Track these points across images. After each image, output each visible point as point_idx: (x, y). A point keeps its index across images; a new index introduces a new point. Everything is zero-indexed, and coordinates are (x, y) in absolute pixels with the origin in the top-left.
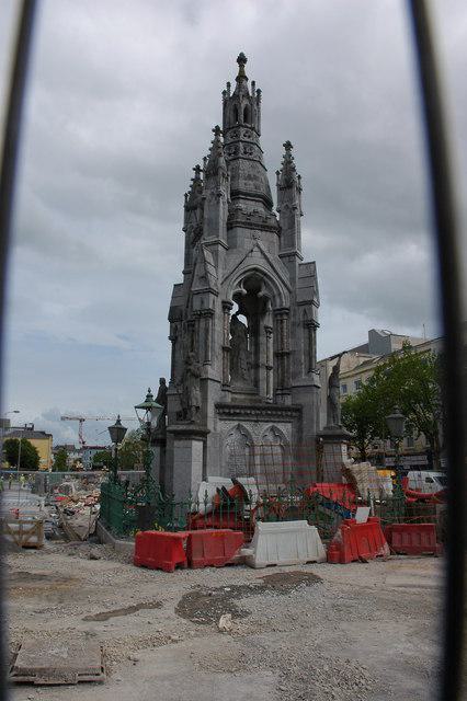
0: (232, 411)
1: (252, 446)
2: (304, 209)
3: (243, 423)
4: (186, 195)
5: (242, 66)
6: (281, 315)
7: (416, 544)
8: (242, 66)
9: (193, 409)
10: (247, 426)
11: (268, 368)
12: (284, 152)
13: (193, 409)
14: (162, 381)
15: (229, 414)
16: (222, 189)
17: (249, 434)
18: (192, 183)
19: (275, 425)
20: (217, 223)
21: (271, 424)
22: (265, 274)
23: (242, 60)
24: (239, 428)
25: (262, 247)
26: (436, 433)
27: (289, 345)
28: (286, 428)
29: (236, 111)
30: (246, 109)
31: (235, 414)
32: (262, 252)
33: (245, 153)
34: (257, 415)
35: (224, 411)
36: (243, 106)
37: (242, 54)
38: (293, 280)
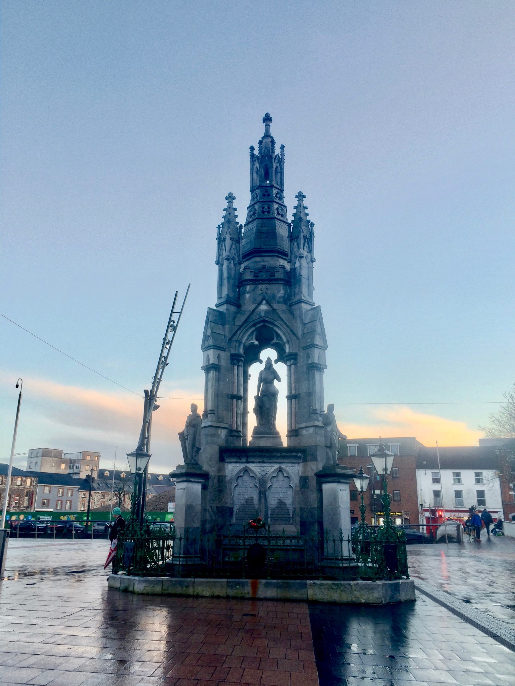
4: (219, 227)
12: (225, 205)
14: (194, 408)
23: (267, 119)
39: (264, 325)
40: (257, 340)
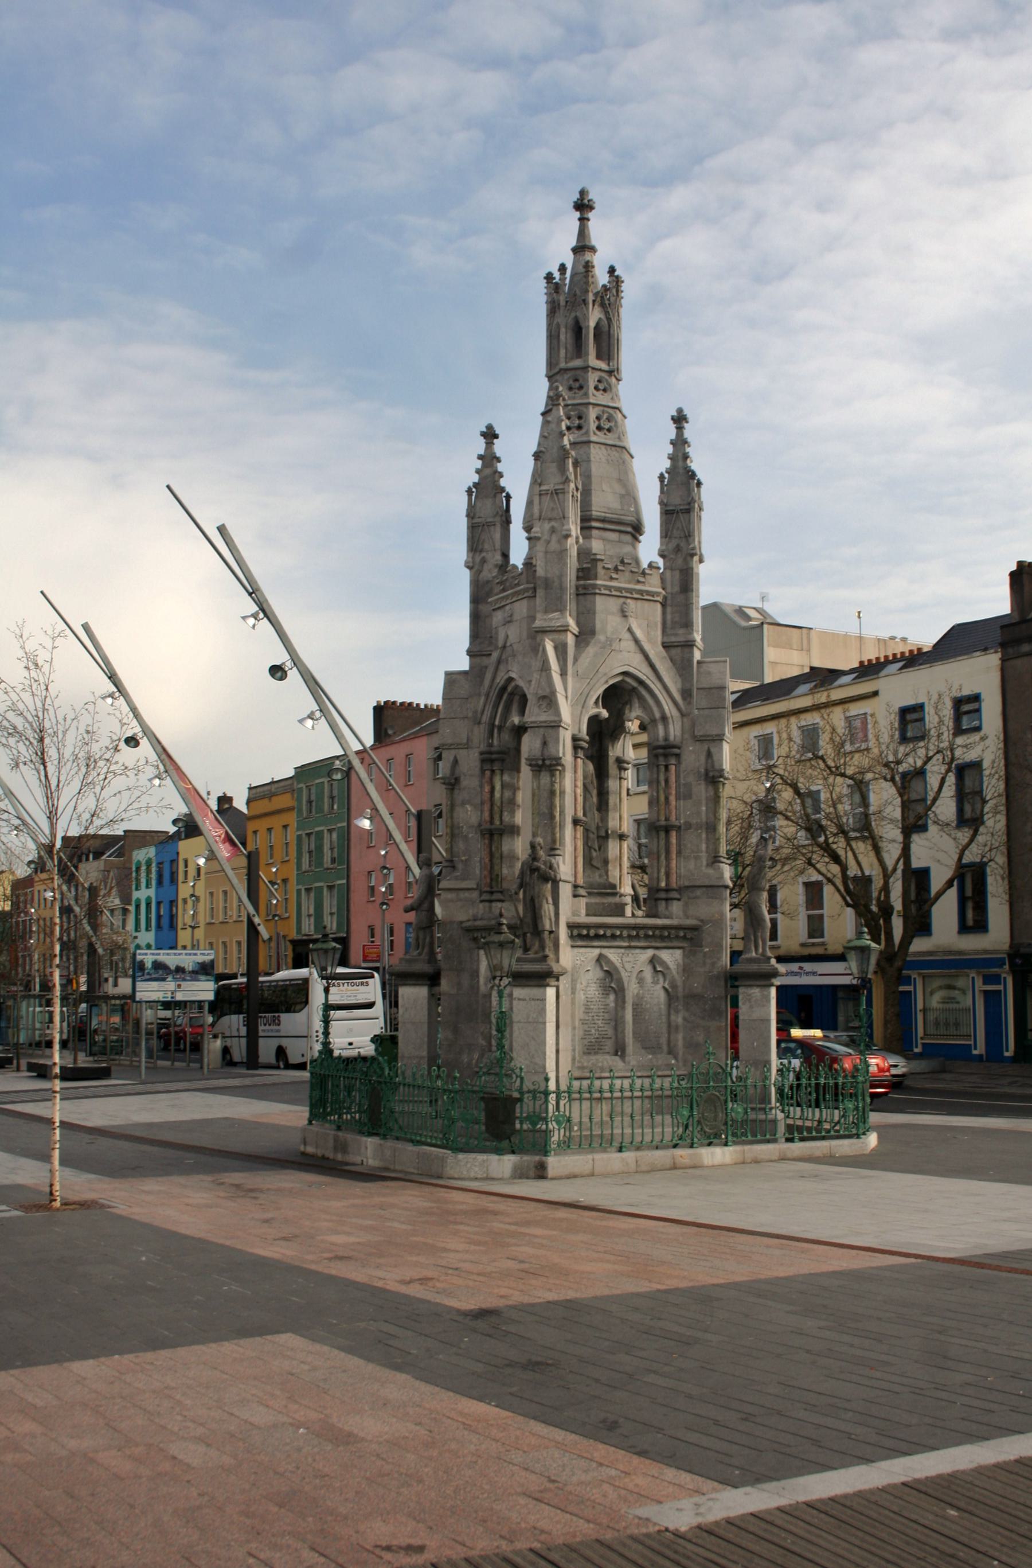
0: (592, 932)
1: (619, 991)
2: (705, 549)
3: (607, 952)
4: (469, 492)
5: (680, 429)
6: (666, 756)
7: (638, 1139)
8: (680, 429)
9: (546, 933)
10: (612, 955)
11: (622, 837)
13: (546, 933)
15: (587, 937)
16: (727, 757)
17: (616, 969)
18: (479, 464)
19: (657, 952)
20: (562, 589)
21: (650, 953)
22: (641, 682)
24: (600, 959)
25: (639, 634)
26: (887, 911)
27: (679, 811)
28: (671, 958)
29: (578, 330)
30: (597, 327)
31: (597, 937)
32: (637, 641)
33: (599, 428)
34: (630, 937)
35: (581, 934)
36: (592, 324)
37: (680, 411)
38: (687, 694)
39: (623, 681)
40: (604, 707)
